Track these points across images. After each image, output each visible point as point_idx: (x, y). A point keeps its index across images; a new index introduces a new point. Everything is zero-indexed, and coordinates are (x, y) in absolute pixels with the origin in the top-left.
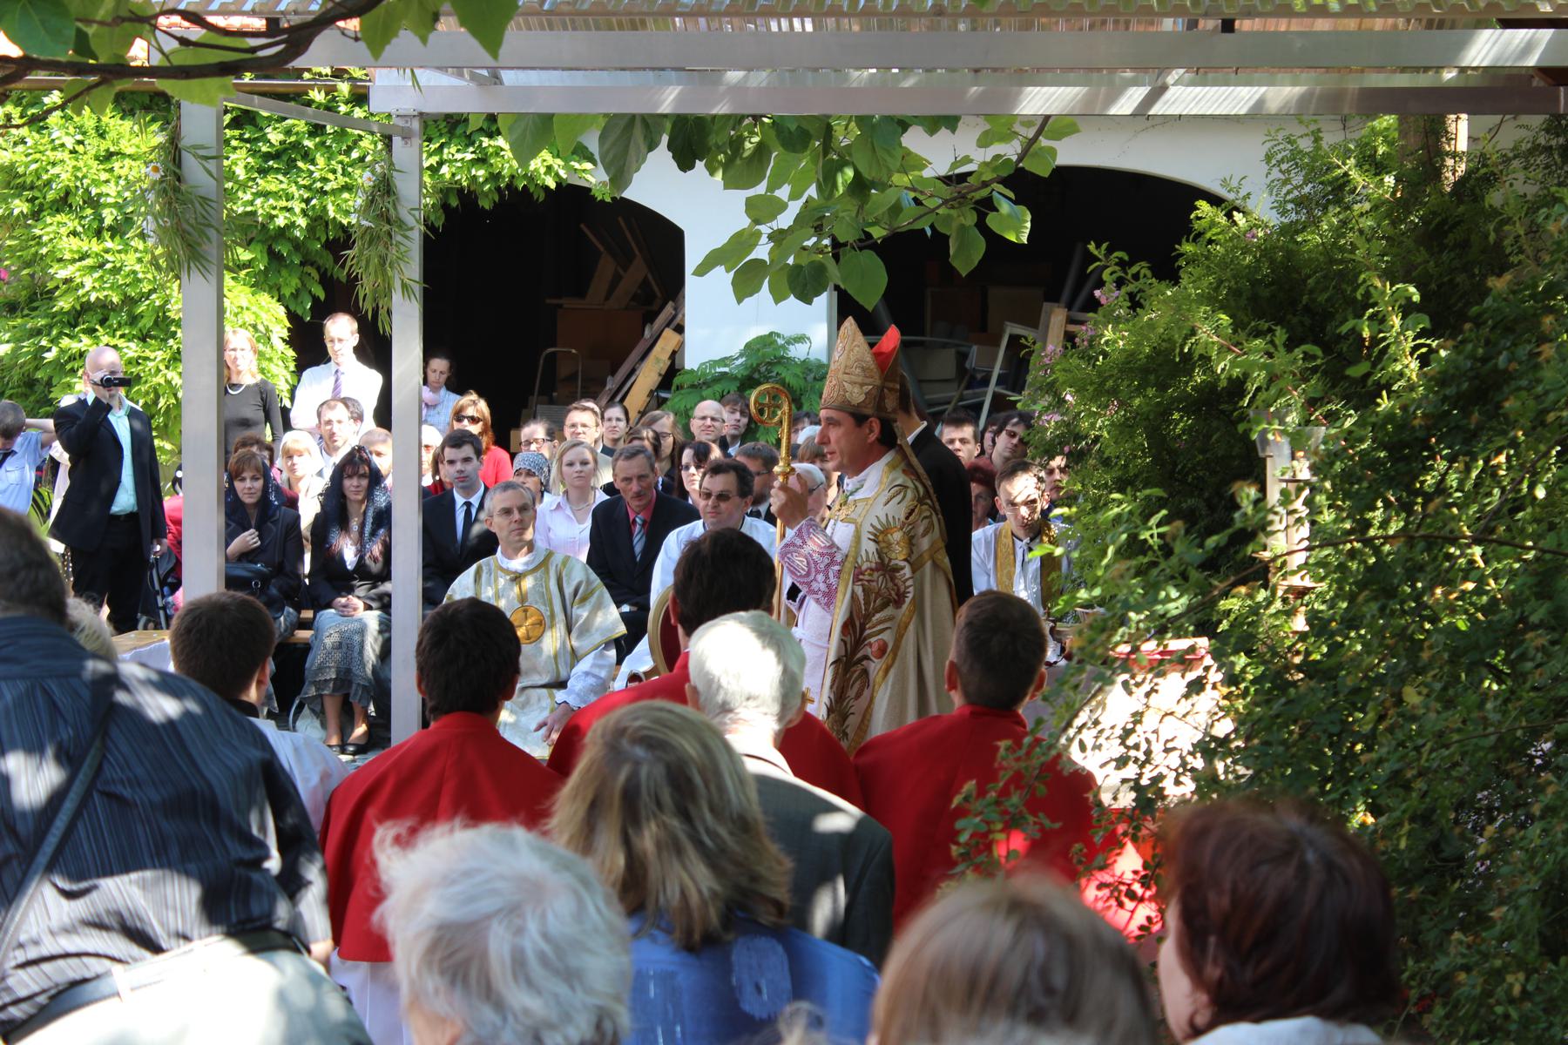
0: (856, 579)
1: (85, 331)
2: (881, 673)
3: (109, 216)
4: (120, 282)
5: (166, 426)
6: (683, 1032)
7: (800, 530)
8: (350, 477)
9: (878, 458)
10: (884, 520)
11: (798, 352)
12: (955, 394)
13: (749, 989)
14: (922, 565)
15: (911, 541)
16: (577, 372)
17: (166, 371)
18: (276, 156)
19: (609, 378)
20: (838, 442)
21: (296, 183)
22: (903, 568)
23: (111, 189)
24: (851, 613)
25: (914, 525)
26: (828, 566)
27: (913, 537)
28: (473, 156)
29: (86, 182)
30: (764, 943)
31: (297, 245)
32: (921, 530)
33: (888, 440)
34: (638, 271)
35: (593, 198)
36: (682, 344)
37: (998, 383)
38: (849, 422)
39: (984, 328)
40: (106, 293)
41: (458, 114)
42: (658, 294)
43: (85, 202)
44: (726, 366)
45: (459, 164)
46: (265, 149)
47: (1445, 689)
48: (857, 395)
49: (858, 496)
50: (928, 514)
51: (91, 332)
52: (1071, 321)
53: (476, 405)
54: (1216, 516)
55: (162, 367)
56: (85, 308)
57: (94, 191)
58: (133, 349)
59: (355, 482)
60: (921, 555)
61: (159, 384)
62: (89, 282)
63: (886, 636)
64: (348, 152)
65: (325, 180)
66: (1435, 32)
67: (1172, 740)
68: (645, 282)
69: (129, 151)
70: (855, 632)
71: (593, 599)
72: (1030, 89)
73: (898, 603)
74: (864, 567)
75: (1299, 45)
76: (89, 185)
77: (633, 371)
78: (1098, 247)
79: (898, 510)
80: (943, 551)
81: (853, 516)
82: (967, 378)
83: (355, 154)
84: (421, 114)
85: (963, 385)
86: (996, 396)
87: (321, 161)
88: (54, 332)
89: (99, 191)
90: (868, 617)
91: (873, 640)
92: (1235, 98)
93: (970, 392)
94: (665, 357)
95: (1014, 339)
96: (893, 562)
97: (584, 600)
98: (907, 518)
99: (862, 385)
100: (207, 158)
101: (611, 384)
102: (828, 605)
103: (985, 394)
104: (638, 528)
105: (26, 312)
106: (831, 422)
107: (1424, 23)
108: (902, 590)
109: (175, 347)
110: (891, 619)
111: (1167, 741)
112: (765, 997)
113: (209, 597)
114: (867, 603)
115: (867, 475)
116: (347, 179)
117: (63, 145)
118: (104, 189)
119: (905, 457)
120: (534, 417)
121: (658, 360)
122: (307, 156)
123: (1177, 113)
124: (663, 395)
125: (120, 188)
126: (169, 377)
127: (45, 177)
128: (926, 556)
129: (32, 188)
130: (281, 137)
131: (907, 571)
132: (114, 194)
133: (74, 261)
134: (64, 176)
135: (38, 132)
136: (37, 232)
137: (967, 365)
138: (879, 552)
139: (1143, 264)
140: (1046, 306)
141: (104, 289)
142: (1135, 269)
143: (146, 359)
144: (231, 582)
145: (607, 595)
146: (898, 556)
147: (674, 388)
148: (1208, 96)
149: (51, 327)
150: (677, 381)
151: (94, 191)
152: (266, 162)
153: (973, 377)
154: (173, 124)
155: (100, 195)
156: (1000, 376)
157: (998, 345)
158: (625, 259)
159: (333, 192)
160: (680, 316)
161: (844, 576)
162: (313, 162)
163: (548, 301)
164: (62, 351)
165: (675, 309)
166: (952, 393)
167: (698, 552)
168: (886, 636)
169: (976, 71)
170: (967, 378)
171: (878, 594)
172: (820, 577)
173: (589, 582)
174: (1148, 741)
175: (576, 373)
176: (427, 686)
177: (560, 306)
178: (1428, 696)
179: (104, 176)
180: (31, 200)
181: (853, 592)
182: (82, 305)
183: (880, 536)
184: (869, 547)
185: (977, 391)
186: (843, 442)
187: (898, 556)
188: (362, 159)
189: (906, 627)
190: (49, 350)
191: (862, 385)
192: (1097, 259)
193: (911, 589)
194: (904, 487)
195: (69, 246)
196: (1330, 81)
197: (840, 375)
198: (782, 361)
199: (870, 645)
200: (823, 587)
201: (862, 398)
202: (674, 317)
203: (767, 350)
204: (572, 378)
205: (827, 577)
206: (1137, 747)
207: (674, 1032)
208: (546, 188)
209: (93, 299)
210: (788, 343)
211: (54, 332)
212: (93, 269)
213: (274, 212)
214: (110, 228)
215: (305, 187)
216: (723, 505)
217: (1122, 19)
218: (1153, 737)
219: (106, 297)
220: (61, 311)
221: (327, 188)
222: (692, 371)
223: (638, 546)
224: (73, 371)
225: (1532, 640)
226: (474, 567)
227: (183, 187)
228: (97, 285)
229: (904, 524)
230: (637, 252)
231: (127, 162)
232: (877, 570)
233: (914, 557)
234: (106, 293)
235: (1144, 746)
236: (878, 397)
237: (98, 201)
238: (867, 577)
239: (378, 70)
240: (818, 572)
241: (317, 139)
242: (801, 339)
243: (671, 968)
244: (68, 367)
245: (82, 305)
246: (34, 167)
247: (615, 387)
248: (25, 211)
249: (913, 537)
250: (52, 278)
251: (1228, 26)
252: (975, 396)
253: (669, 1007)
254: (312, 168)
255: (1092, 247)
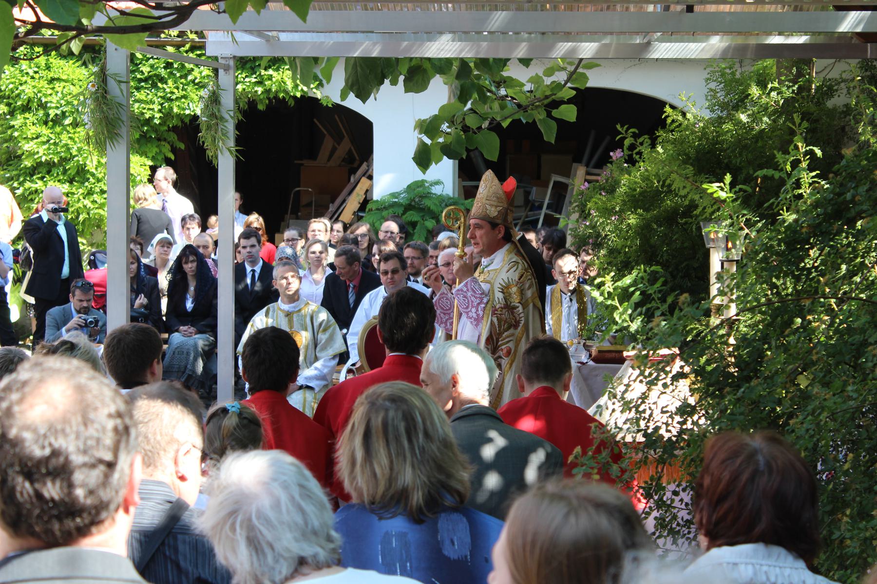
0: (493, 314)
1: (39, 179)
2: (508, 366)
3: (52, 113)
4: (59, 150)
5: (83, 230)
6: (411, 567)
7: (467, 283)
8: (186, 263)
9: (501, 247)
10: (506, 281)
11: (437, 190)
12: (523, 214)
13: (447, 543)
14: (528, 305)
15: (522, 292)
16: (312, 202)
17: (83, 200)
18: (146, 80)
19: (331, 205)
20: (481, 237)
21: (156, 95)
22: (518, 307)
23: (54, 99)
24: (491, 332)
25: (523, 283)
26: (479, 304)
27: (523, 290)
28: (256, 80)
29: (39, 95)
30: (455, 516)
31: (155, 128)
32: (527, 286)
33: (508, 238)
34: (346, 145)
35: (321, 105)
36: (372, 186)
37: (548, 208)
38: (487, 226)
39: (539, 177)
40: (51, 156)
41: (247, 57)
42: (357, 158)
43: (38, 106)
44: (396, 198)
45: (248, 84)
46: (139, 76)
47: (825, 376)
48: (493, 212)
49: (490, 268)
50: (530, 277)
51: (42, 178)
52: (588, 173)
53: (256, 220)
54: (676, 281)
55: (81, 197)
56: (40, 164)
57: (44, 100)
58: (65, 188)
59: (190, 265)
60: (527, 300)
61: (80, 208)
62: (42, 150)
63: (511, 345)
64: (185, 76)
65: (172, 93)
66: (798, 12)
67: (666, 407)
68: (350, 151)
69: (64, 77)
70: (493, 343)
71: (330, 330)
72: (561, 43)
73: (516, 326)
74: (497, 307)
75: (728, 20)
76: (41, 97)
77: (344, 201)
78: (622, 126)
79: (514, 275)
80: (538, 299)
81: (488, 279)
82: (530, 205)
83: (190, 78)
84: (234, 57)
85: (528, 208)
86: (546, 215)
87: (170, 82)
88: (21, 179)
89: (46, 100)
90: (500, 334)
91: (503, 347)
92: (692, 49)
93: (532, 213)
94: (362, 193)
95: (556, 183)
96: (512, 304)
97: (325, 330)
98: (519, 279)
99: (496, 207)
100: (120, 82)
101: (332, 208)
102: (477, 325)
103: (540, 214)
104: (351, 290)
105: (5, 167)
106: (477, 226)
107: (793, 7)
108: (518, 319)
109: (89, 186)
110: (513, 335)
111: (663, 408)
112: (456, 547)
113: (123, 326)
114: (500, 326)
115: (495, 256)
116: (184, 92)
117: (27, 73)
118: (49, 99)
119: (516, 246)
120: (288, 227)
121: (358, 195)
122: (163, 80)
123: (656, 57)
124: (361, 214)
125: (58, 99)
126: (85, 204)
127: (17, 92)
128: (530, 300)
129: (9, 98)
130: (149, 69)
131: (520, 309)
132: (55, 102)
133: (33, 139)
134: (28, 91)
135: (12, 66)
136: (12, 123)
137: (530, 198)
138: (505, 298)
139: (646, 136)
140: (574, 165)
141: (49, 154)
142: (641, 140)
143: (73, 194)
144: (133, 319)
145: (337, 326)
146: (515, 300)
147: (367, 210)
148: (674, 47)
149: (19, 176)
150: (369, 206)
151: (44, 100)
152: (140, 83)
153: (533, 205)
154: (102, 61)
155: (46, 103)
156: (548, 204)
157: (547, 187)
158: (339, 139)
159: (177, 98)
160: (370, 170)
161: (487, 312)
162: (166, 83)
163: (296, 162)
164: (25, 190)
165: (368, 166)
166: (522, 213)
167: (389, 302)
168: (511, 345)
169: (543, 34)
170: (530, 205)
171: (505, 322)
172: (474, 310)
173: (328, 321)
174: (650, 408)
175: (311, 202)
176: (248, 377)
177: (302, 164)
178: (813, 380)
179: (50, 91)
180: (8, 105)
181: (492, 320)
182: (37, 163)
183: (505, 290)
184: (499, 295)
185: (536, 212)
186: (484, 239)
187: (515, 300)
188: (193, 81)
189: (520, 340)
190: (18, 188)
191: (496, 207)
192: (620, 133)
193: (523, 319)
194: (517, 263)
195: (32, 130)
196: (740, 40)
197: (484, 201)
198: (428, 195)
199: (502, 350)
200: (475, 315)
201: (496, 214)
202: (367, 171)
203: (421, 189)
204: (309, 205)
205: (477, 310)
206: (644, 411)
207: (406, 566)
208: (295, 97)
209: (43, 159)
210: (431, 185)
211: (21, 179)
212: (44, 143)
213: (144, 111)
214: (52, 120)
215: (161, 97)
216: (396, 276)
217: (612, 4)
218: (653, 407)
219: (51, 158)
220: (26, 168)
221: (174, 97)
222: (377, 201)
223: (352, 298)
224: (32, 200)
225: (872, 351)
226: (266, 308)
227: (108, 97)
228: (45, 152)
229: (518, 282)
230: (345, 134)
231: (63, 84)
232: (505, 308)
233: (524, 301)
234: (51, 156)
235: (648, 412)
236: (504, 214)
237: (46, 106)
238: (499, 312)
239: (210, 32)
240: (473, 307)
241: (168, 70)
242: (438, 183)
243: (404, 530)
244: (29, 198)
245: (37, 163)
246: (11, 86)
247: (334, 210)
248: (6, 111)
249: (523, 290)
250: (20, 148)
251: (690, 9)
252: (534, 215)
253: (403, 552)
254: (165, 86)
255: (618, 127)
